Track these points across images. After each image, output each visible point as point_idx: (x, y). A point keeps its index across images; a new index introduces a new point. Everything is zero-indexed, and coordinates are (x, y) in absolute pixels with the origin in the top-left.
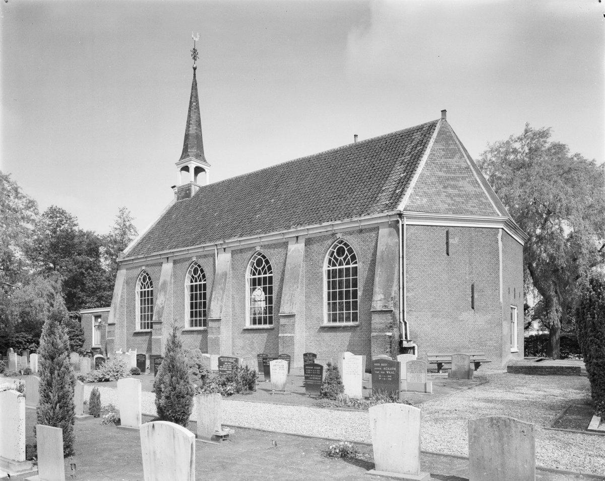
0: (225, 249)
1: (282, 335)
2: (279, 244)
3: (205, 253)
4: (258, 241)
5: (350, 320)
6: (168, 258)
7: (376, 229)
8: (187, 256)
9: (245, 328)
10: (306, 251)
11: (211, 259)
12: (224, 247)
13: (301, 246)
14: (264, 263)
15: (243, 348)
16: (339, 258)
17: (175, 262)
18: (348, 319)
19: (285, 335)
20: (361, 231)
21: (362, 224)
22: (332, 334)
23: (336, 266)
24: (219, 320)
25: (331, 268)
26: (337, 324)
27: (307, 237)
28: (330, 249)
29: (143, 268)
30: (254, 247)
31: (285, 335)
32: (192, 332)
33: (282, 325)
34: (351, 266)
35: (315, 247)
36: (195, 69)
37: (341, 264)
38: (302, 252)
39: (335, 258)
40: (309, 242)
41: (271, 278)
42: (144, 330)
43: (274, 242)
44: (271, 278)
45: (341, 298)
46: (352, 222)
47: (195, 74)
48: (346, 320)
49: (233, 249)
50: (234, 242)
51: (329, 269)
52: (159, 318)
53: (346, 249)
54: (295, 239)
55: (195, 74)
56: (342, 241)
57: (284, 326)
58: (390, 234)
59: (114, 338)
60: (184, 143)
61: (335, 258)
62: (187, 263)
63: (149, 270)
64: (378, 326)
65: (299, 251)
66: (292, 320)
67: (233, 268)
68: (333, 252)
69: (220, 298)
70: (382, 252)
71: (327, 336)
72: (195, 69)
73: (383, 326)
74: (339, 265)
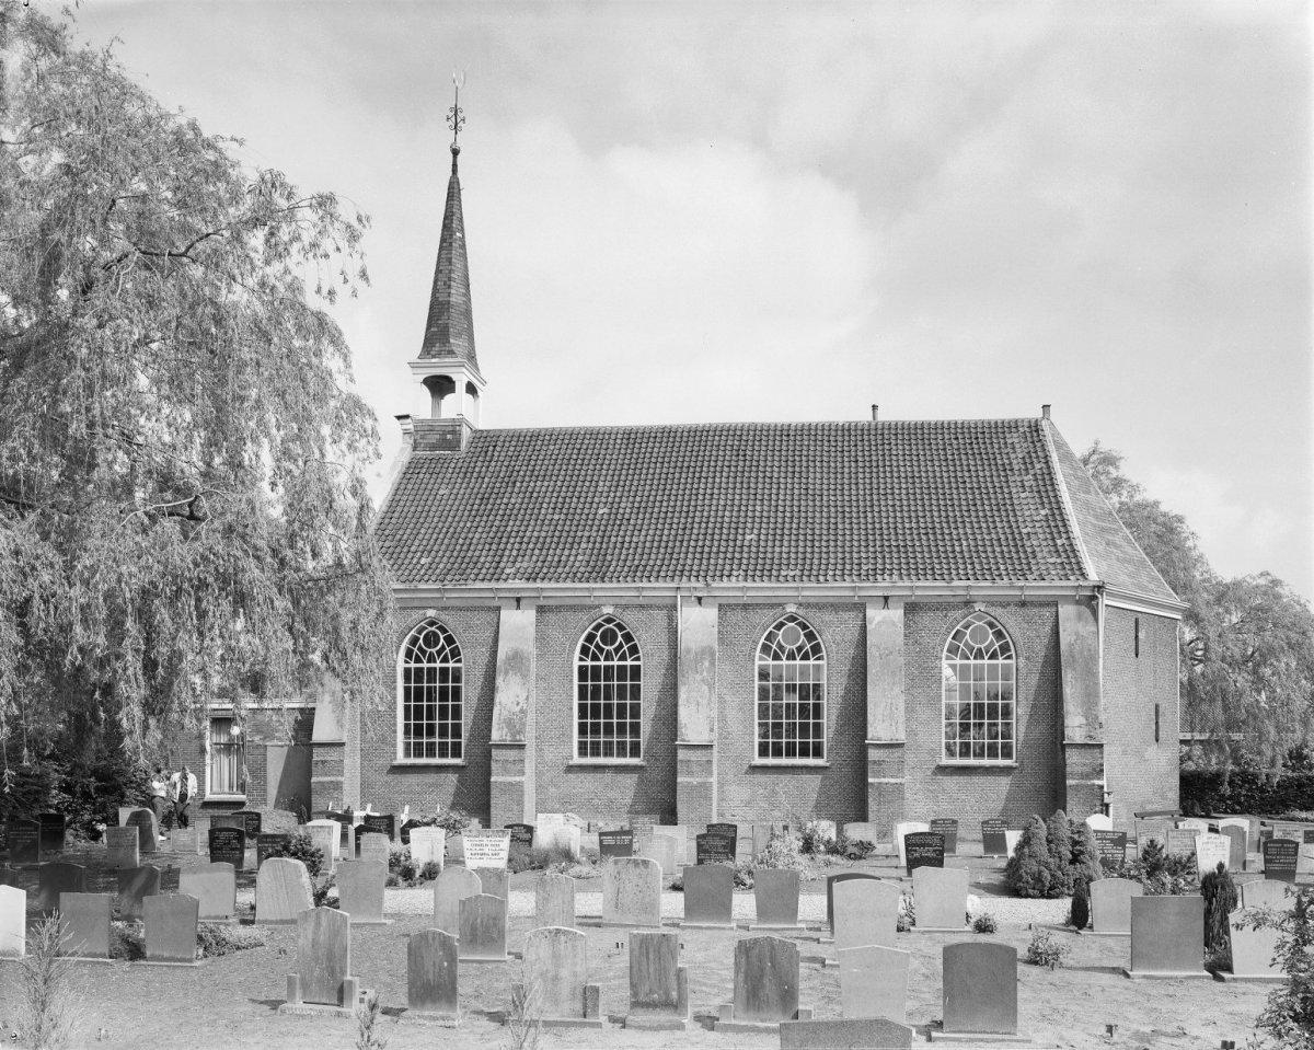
0: (699, 599)
1: (877, 780)
2: (847, 605)
3: (641, 601)
4: (609, 595)
5: (794, 755)
6: (518, 600)
7: (1053, 603)
8: (588, 602)
9: (396, 763)
10: (907, 626)
11: (661, 615)
12: (700, 595)
13: (896, 614)
14: (442, 640)
15: (748, 804)
16: (606, 648)
17: (541, 610)
18: (622, 753)
19: (886, 780)
20: (1023, 604)
21: (918, 593)
22: (963, 779)
23: (599, 660)
24: (709, 747)
25: (413, 665)
26: (424, 761)
27: (909, 600)
28: (412, 632)
29: (431, 613)
30: (780, 605)
31: (886, 780)
32: (582, 768)
33: (875, 762)
34: (451, 665)
35: (926, 619)
36: (455, 153)
37: (431, 659)
38: (532, 630)
39: (420, 649)
40: (912, 608)
41: (457, 671)
42: (412, 761)
43: (832, 600)
44: (636, 672)
45: (430, 717)
46: (1012, 587)
47: (455, 165)
48: (975, 755)
49: (724, 601)
50: (732, 587)
51: (407, 665)
52: (513, 735)
53: (619, 634)
54: (882, 600)
55: (455, 165)
56: (796, 619)
57: (878, 763)
58: (1079, 617)
59: (340, 778)
60: (428, 329)
61: (420, 649)
62: (584, 617)
63: (449, 620)
64: (1079, 769)
65: (894, 624)
66: (897, 753)
67: (721, 640)
68: (595, 636)
69: (705, 702)
70: (1071, 645)
71: (951, 782)
72: (455, 153)
73: (1087, 769)
74: (429, 662)
